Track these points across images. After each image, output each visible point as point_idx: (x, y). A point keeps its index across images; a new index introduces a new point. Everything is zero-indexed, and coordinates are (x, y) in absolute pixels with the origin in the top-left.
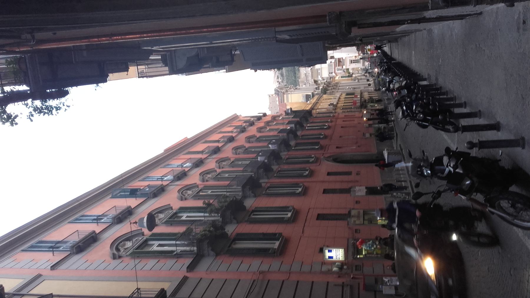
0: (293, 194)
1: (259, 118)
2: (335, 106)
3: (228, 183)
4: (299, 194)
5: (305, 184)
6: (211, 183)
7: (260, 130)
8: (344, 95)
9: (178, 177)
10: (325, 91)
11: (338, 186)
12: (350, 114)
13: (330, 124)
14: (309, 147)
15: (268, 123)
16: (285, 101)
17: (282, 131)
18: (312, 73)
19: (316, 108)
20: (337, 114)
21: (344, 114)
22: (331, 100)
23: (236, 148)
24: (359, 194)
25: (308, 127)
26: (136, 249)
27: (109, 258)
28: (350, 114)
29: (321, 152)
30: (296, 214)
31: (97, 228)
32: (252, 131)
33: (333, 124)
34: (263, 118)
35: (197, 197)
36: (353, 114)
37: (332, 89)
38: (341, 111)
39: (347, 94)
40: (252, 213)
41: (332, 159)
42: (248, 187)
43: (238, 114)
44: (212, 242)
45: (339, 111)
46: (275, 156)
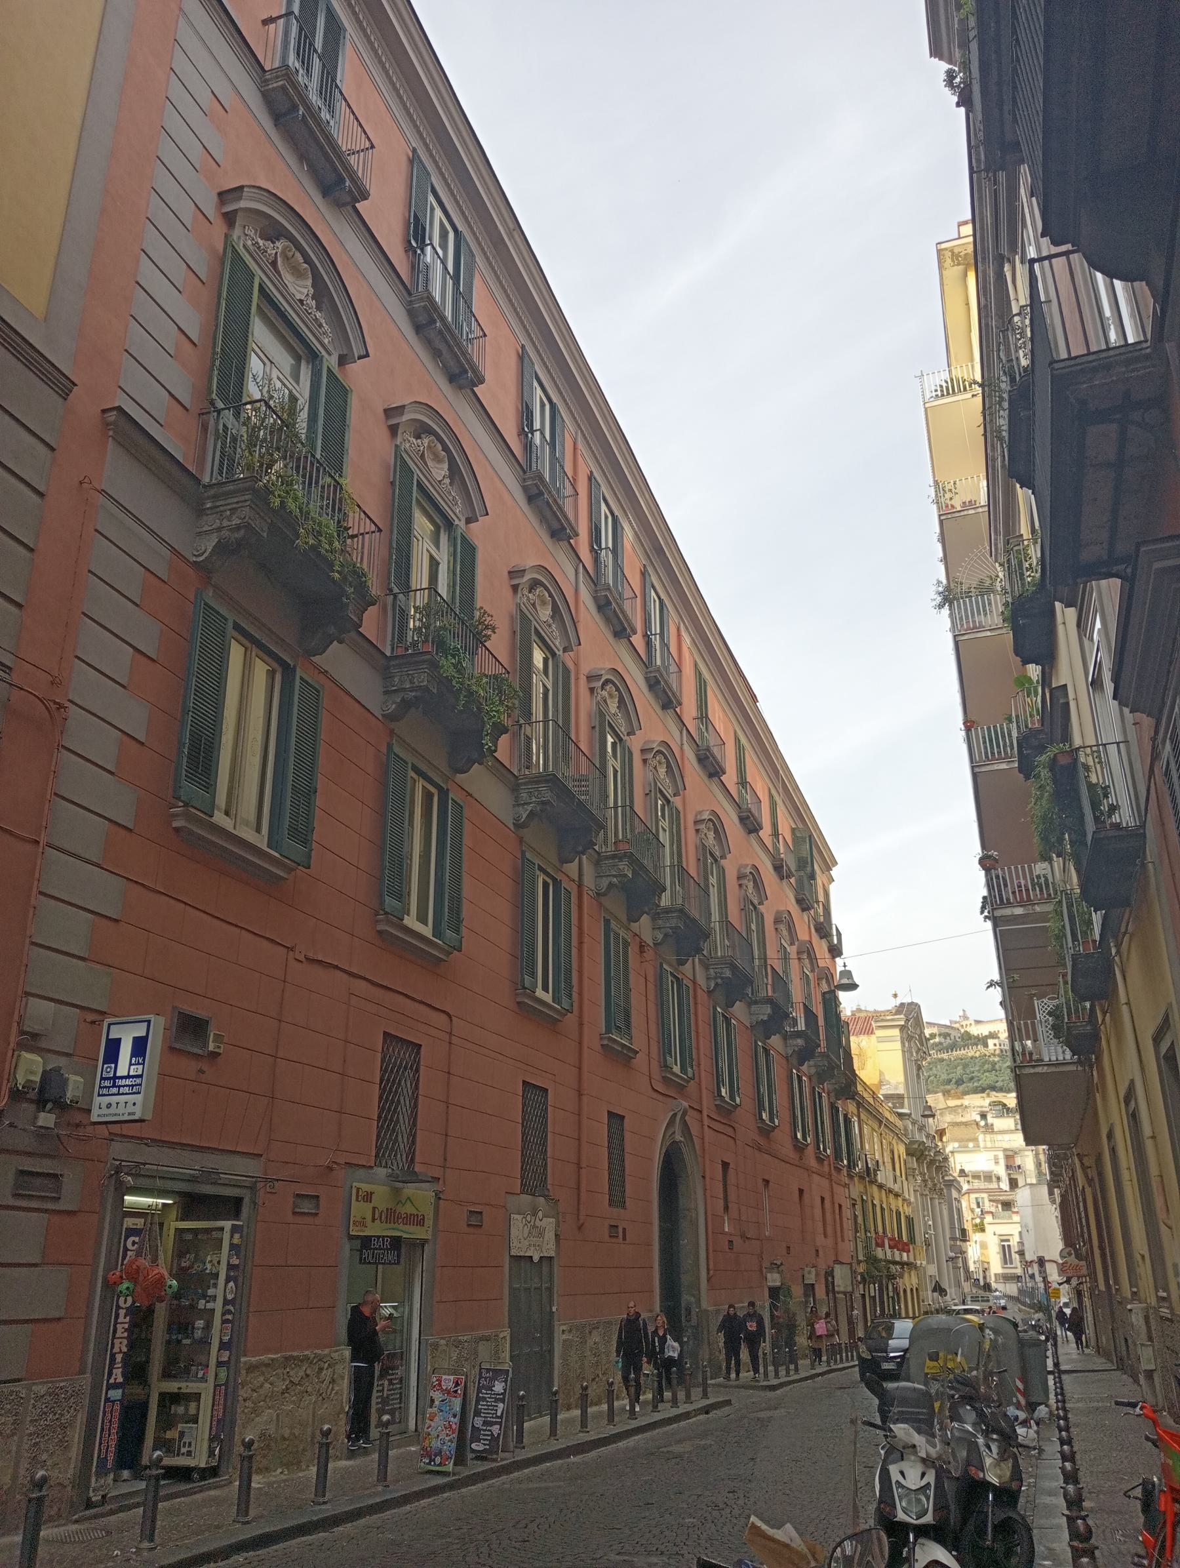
0: (523, 960)
1: (824, 929)
2: (869, 1175)
3: (693, 871)
4: (521, 989)
5: (571, 1020)
6: (690, 839)
7: (784, 920)
8: (906, 1210)
9: (609, 603)
10: (917, 1152)
11: (558, 1147)
12: (848, 1225)
13: (810, 1150)
14: (574, 951)
15: (808, 952)
16: (879, 1033)
17: (781, 982)
18: (966, 1124)
19: (862, 1116)
20: (847, 1180)
21: (847, 1204)
22: (889, 1166)
23: (756, 877)
24: (519, 1227)
25: (800, 1078)
26: (262, 288)
27: (516, 562)
28: (848, 1225)
29: (707, 1104)
30: (431, 960)
31: (689, 709)
32: (780, 897)
33: (813, 1163)
34: (824, 944)
35: (602, 724)
36: (849, 1234)
37: (922, 1174)
38: (855, 1195)
39: (910, 1221)
40: (554, 879)
41: (678, 1137)
42: (548, 796)
43: (834, 872)
44: (274, 560)
45: (856, 1189)
46: (689, 937)
